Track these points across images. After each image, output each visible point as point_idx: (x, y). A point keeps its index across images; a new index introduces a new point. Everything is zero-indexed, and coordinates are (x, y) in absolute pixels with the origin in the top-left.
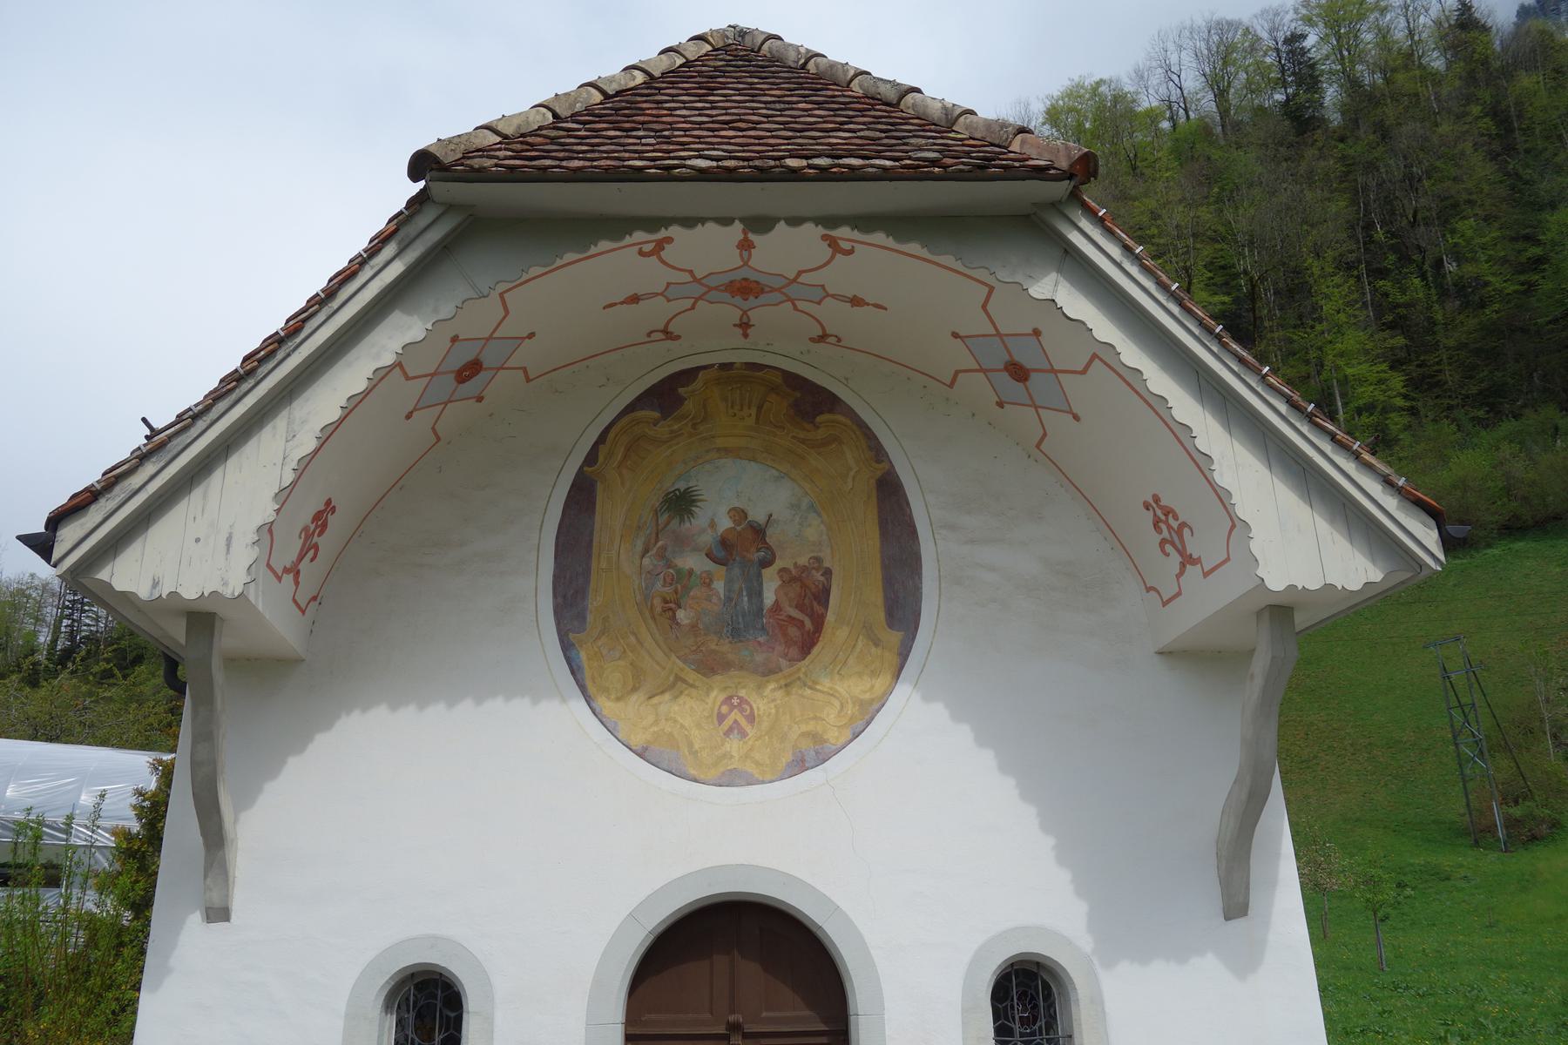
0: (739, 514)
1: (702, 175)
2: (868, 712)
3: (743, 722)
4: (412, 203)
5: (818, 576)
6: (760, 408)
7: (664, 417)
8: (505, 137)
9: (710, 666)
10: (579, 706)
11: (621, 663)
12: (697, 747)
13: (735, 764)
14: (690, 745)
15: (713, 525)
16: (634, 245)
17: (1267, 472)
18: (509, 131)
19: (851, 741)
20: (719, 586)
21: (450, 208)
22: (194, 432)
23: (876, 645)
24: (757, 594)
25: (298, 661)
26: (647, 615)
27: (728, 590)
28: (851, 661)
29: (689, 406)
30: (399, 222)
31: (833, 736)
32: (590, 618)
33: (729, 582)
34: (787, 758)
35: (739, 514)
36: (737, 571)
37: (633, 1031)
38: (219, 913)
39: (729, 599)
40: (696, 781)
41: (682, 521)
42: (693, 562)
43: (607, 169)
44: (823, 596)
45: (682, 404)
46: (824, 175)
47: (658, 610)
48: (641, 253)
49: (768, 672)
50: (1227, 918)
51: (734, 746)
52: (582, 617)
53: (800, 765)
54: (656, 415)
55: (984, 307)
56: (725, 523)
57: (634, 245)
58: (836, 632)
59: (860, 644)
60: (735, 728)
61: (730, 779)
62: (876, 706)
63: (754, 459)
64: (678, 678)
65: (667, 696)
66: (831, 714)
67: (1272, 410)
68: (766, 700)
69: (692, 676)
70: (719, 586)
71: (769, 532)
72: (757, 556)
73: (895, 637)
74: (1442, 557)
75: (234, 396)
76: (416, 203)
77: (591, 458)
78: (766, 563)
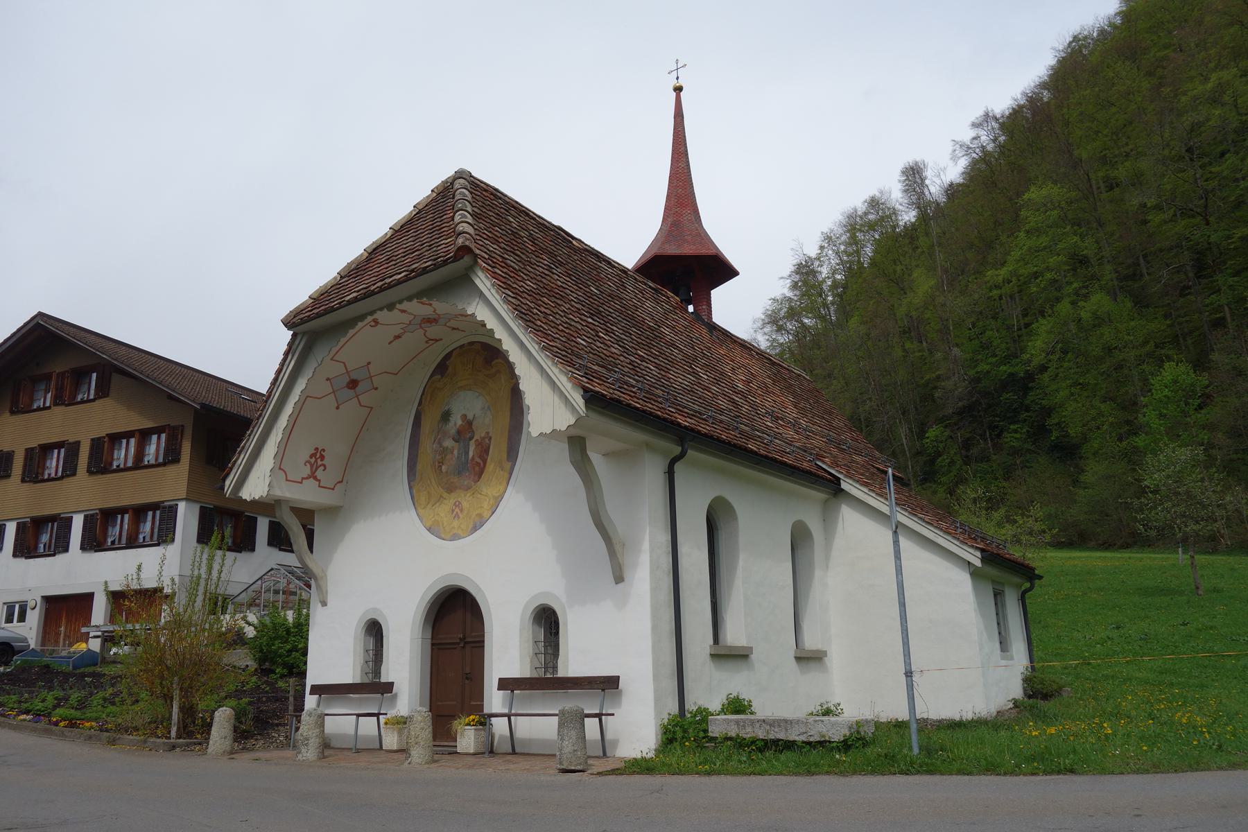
0: (464, 417)
1: (356, 300)
2: (498, 500)
3: (459, 512)
4: (292, 335)
5: (487, 441)
6: (473, 364)
7: (442, 376)
8: (315, 299)
9: (450, 489)
10: (413, 512)
11: (425, 492)
12: (445, 525)
13: (455, 531)
14: (443, 524)
15: (455, 424)
16: (367, 324)
17: (540, 377)
18: (315, 297)
19: (491, 516)
20: (456, 452)
21: (304, 333)
22: (251, 440)
23: (502, 470)
24: (467, 453)
25: (341, 507)
26: (434, 470)
27: (458, 454)
28: (494, 479)
29: (450, 370)
30: (290, 345)
31: (486, 514)
32: (417, 474)
33: (459, 450)
34: (471, 526)
35: (464, 417)
36: (462, 444)
37: (434, 642)
38: (324, 604)
39: (458, 457)
40: (443, 539)
41: (446, 425)
42: (448, 443)
43: (325, 310)
44: (487, 451)
45: (447, 369)
46: (382, 289)
47: (437, 467)
48: (371, 326)
49: (468, 488)
50: (616, 583)
51: (456, 523)
52: (415, 475)
53: (475, 529)
54: (439, 377)
55: (344, 363)
56: (460, 422)
57: (367, 324)
58: (490, 467)
59: (497, 471)
60: (457, 516)
61: (455, 537)
62: (499, 500)
63: (470, 390)
64: (441, 496)
65: (438, 504)
66: (485, 505)
67: (533, 348)
68: (466, 500)
69: (445, 495)
70: (456, 452)
71: (474, 423)
72: (468, 436)
73: (508, 465)
74: (584, 409)
75: (258, 424)
76: (294, 336)
77: (420, 404)
78: (471, 439)
